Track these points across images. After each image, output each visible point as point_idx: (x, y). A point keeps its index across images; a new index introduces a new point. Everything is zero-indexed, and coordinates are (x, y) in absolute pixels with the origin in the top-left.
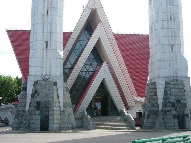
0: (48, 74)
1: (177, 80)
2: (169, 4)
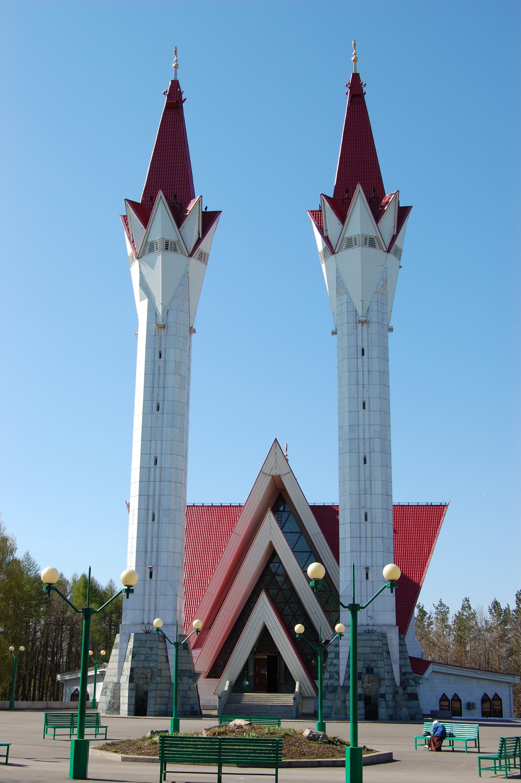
1: (373, 631)
2: (363, 492)
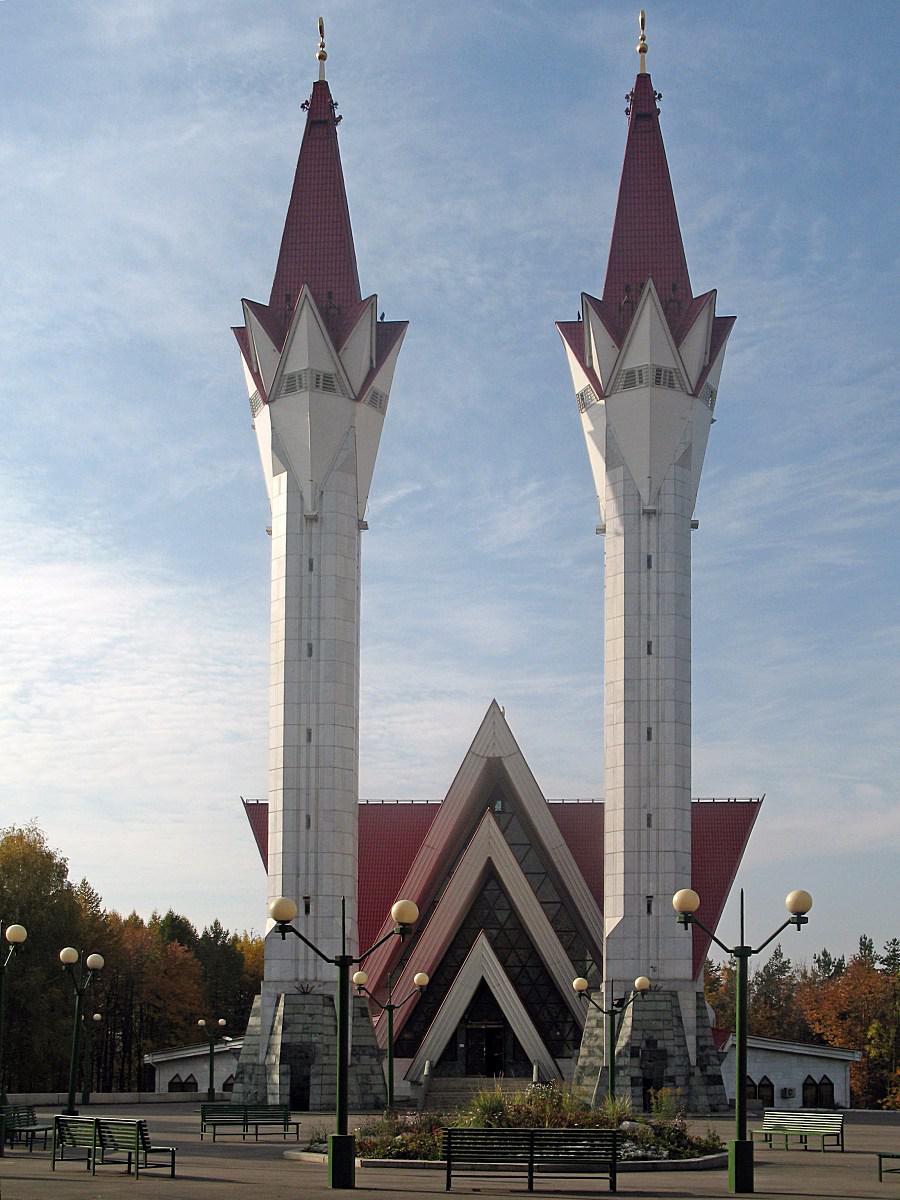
0: (311, 977)
